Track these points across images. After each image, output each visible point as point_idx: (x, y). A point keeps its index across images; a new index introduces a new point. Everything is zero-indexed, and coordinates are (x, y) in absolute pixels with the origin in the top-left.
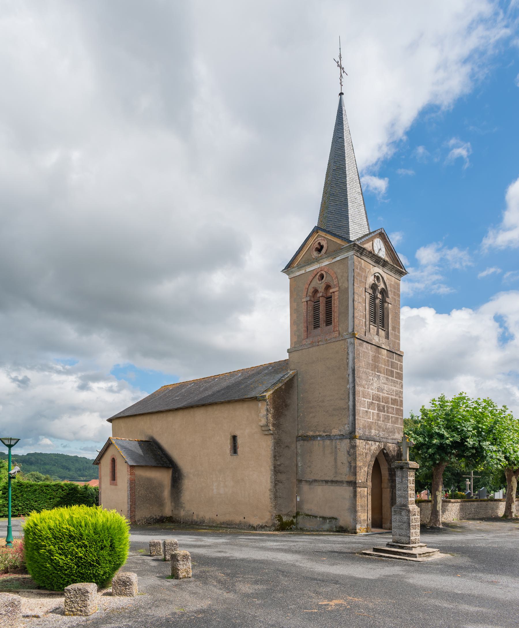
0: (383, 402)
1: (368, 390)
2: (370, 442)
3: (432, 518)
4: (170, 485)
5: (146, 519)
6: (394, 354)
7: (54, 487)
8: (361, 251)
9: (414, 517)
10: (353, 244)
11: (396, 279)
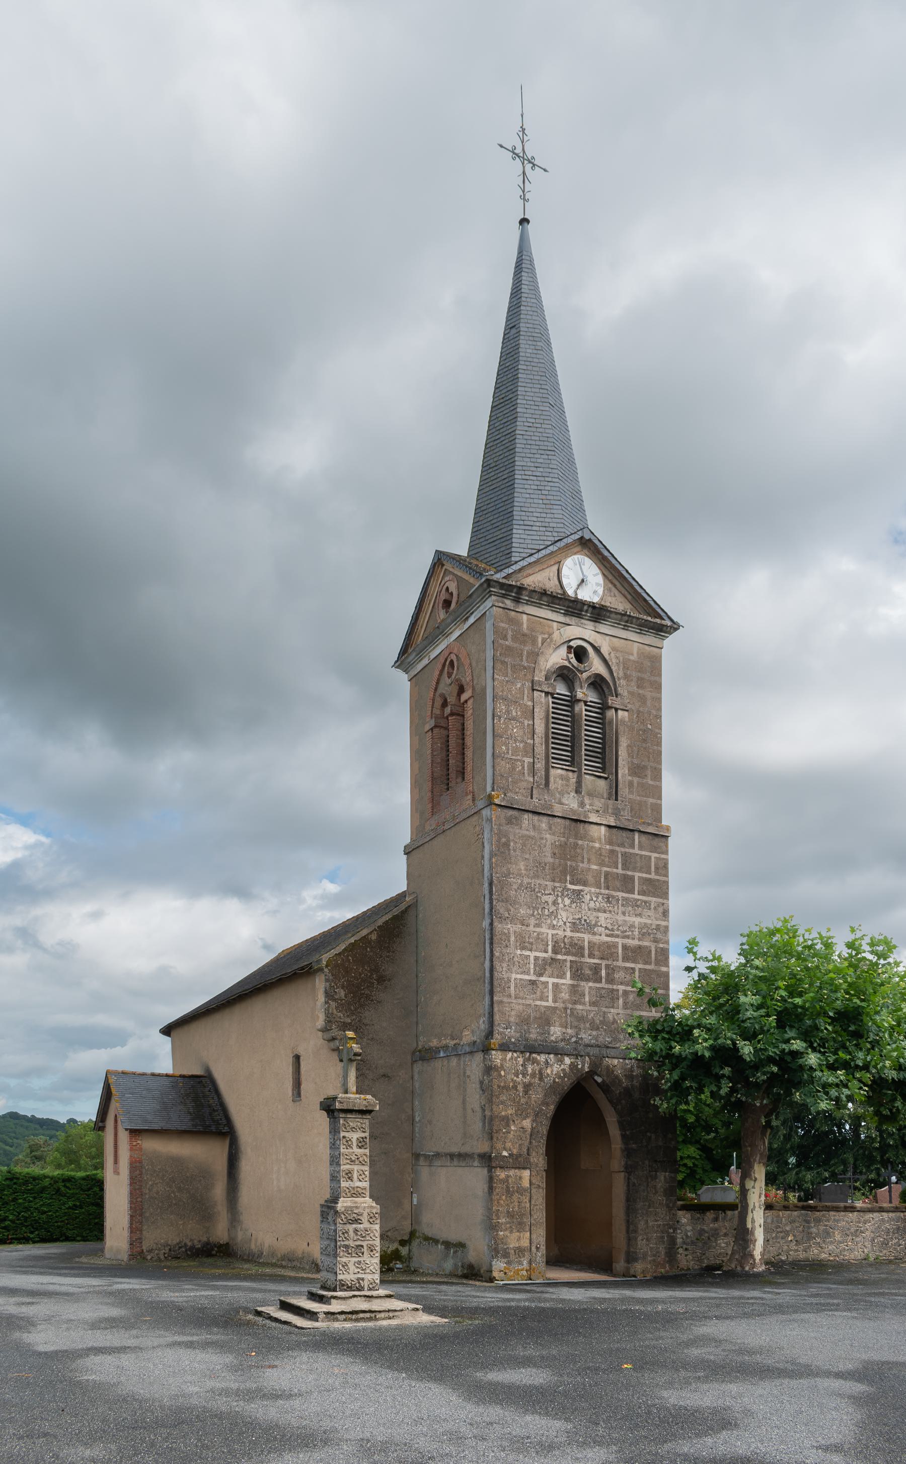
0: (591, 955)
1: (538, 930)
2: (542, 1058)
3: (735, 1248)
4: (226, 1171)
5: (167, 1249)
6: (637, 835)
7: (82, 1182)
8: (513, 594)
9: (354, 1226)
10: (484, 581)
11: (647, 647)
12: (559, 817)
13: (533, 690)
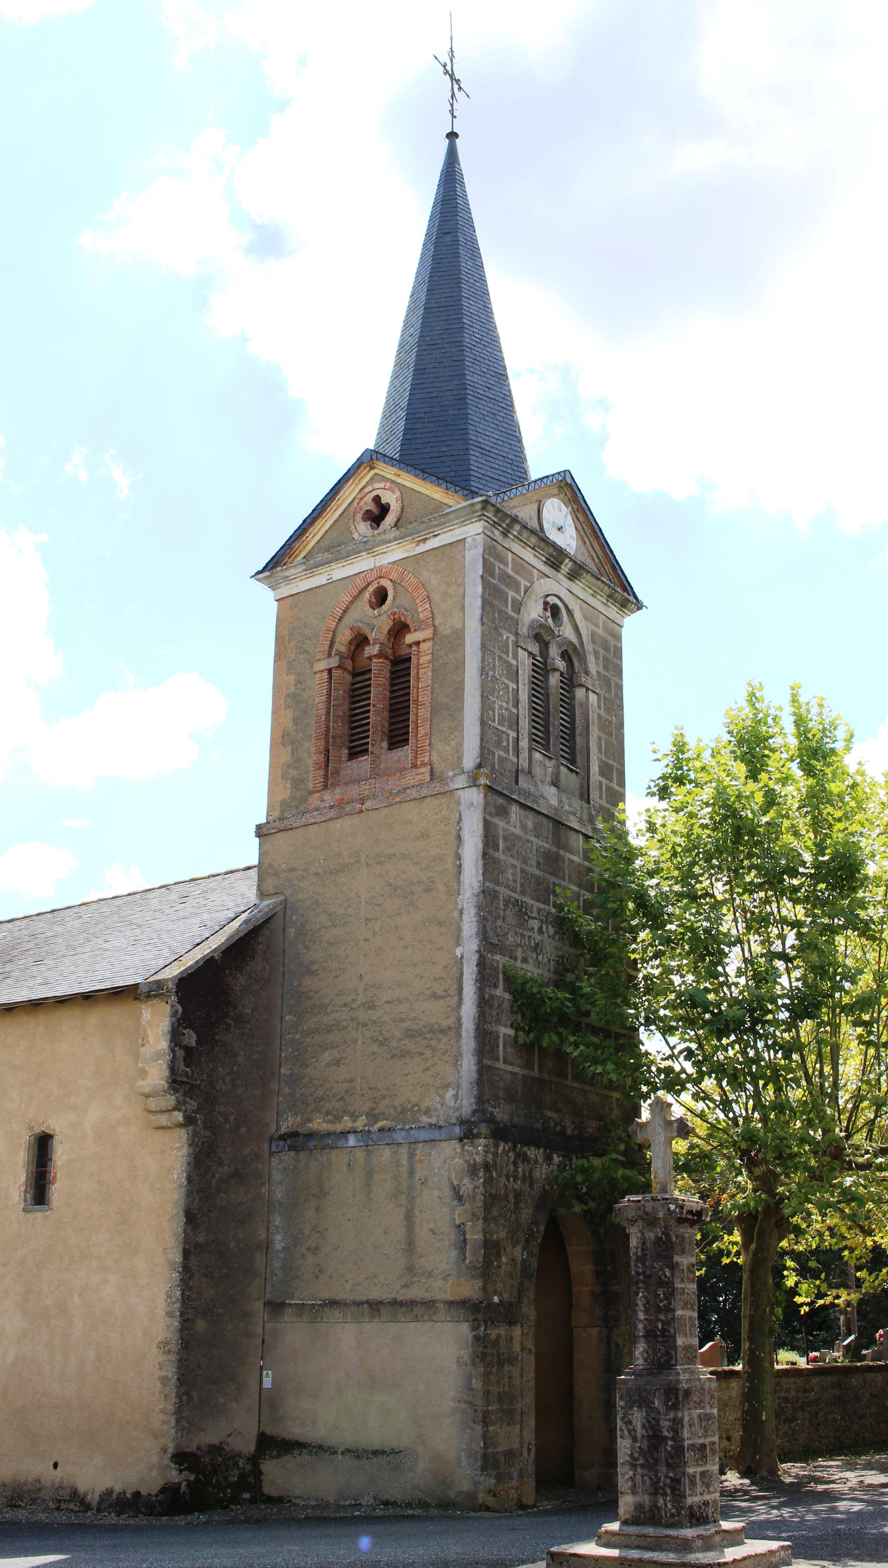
12: (543, 814)
13: (518, 646)
